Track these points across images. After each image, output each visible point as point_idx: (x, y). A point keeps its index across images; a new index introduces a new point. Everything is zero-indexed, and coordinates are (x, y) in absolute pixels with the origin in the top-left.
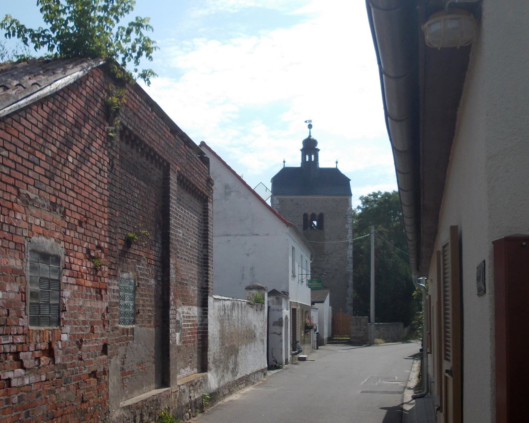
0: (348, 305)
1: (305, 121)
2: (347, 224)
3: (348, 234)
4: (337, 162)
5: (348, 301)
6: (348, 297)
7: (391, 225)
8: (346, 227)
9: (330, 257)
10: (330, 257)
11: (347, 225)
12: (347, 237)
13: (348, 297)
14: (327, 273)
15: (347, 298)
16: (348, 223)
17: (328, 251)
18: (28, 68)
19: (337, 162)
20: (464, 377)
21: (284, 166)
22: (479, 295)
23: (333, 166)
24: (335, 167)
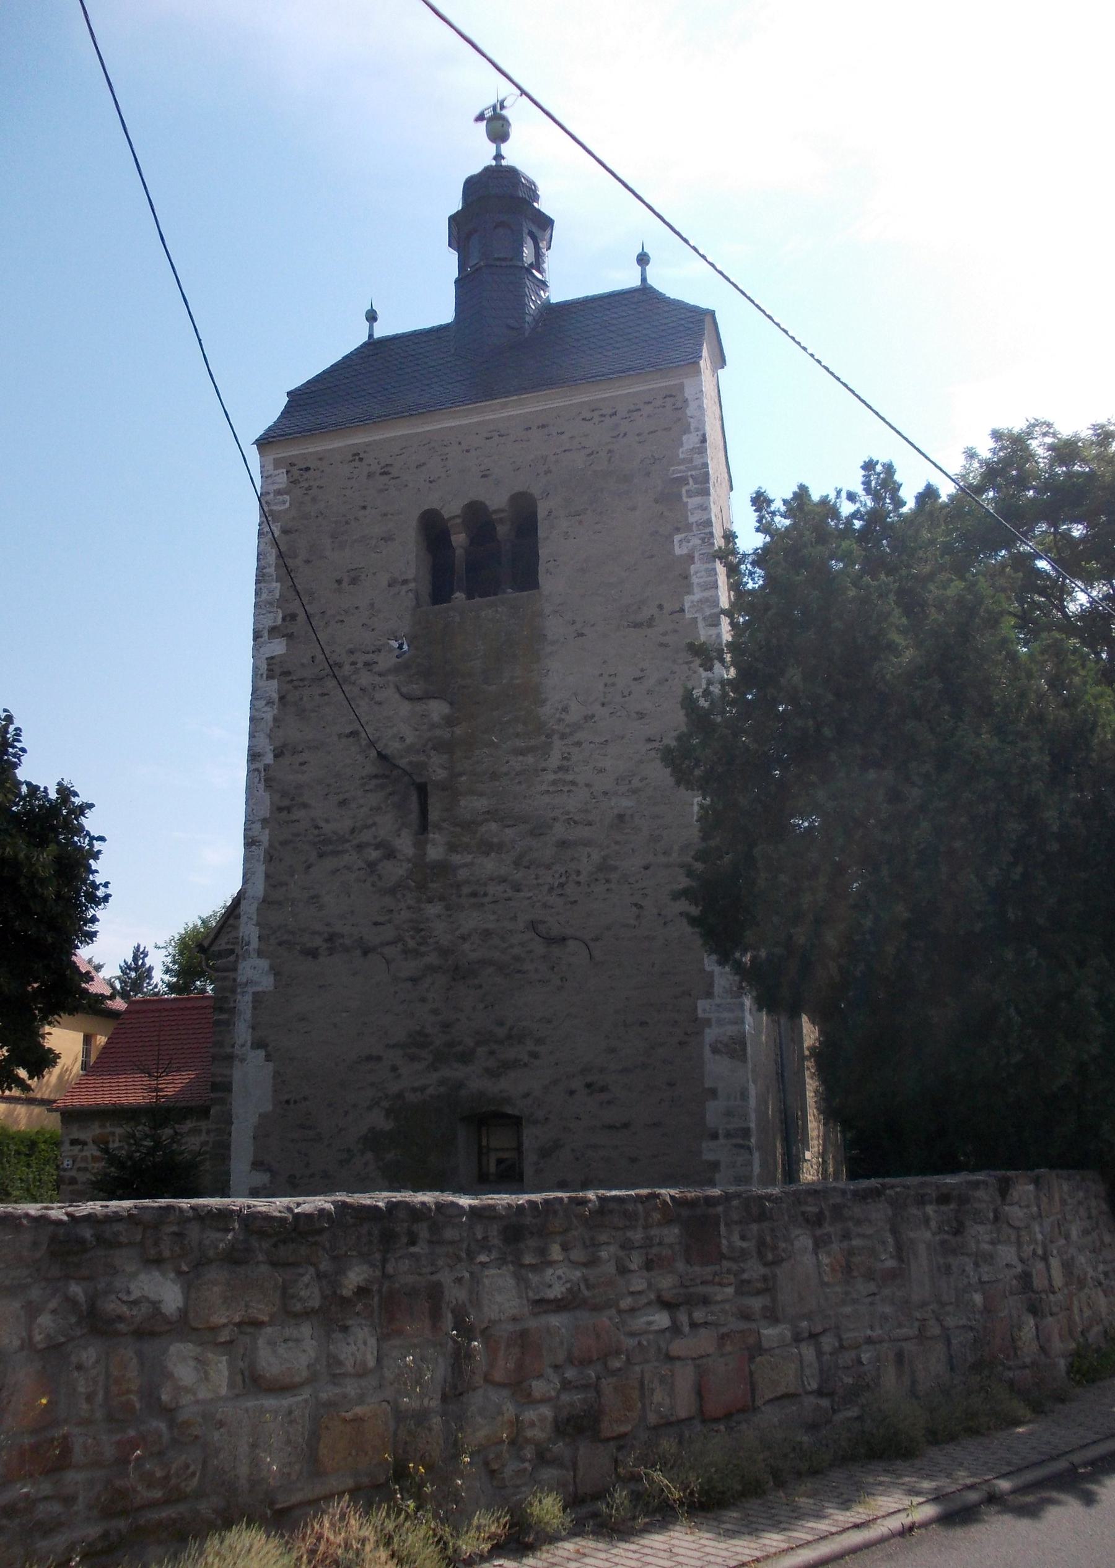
0: (715, 1051)
1: (477, 113)
2: (678, 530)
3: (690, 592)
4: (643, 259)
5: (708, 1022)
6: (709, 994)
7: (1054, 672)
8: (678, 551)
9: (578, 744)
10: (578, 744)
11: (677, 538)
12: (682, 610)
13: (709, 994)
14: (563, 844)
15: (701, 1004)
16: (688, 527)
17: (565, 710)
18: (958, 844)
19: (643, 259)
20: (590, 293)
21: (371, 336)
22: (153, 968)
23: (627, 278)
24: (636, 282)
